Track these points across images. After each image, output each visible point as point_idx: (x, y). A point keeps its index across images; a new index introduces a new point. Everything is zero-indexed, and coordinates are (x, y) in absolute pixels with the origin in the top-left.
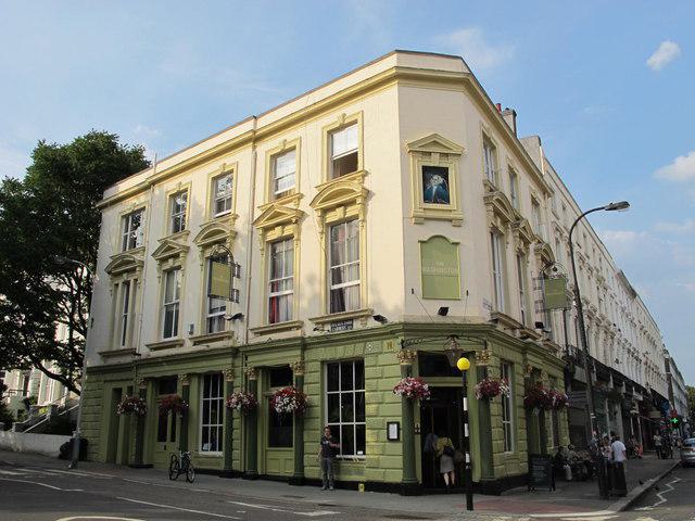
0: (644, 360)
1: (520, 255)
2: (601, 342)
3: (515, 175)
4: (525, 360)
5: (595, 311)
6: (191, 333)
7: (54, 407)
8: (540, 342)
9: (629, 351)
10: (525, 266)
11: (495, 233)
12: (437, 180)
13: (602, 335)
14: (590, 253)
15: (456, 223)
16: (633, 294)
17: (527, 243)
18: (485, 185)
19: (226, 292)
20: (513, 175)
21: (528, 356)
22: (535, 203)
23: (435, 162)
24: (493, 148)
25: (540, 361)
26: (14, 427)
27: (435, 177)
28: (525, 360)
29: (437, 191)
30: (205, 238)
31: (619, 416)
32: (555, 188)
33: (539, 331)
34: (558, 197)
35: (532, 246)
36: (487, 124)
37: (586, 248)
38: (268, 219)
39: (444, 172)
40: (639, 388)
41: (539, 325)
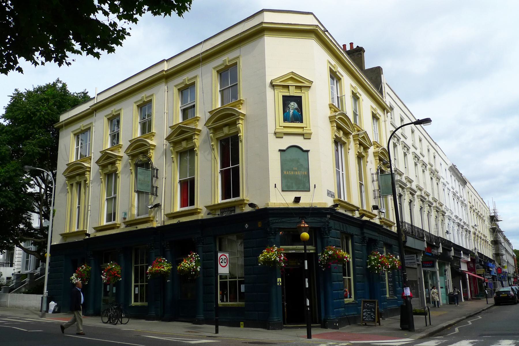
0: (472, 230)
1: (360, 157)
2: (433, 218)
3: (358, 98)
4: (363, 233)
5: (428, 196)
6: (125, 218)
7: (31, 274)
8: (376, 221)
9: (459, 225)
10: (365, 166)
11: (337, 142)
12: (293, 105)
13: (433, 213)
14: (425, 152)
15: (306, 136)
16: (464, 182)
17: (366, 148)
18: (330, 108)
19: (149, 190)
20: (355, 97)
21: (365, 231)
22: (375, 117)
23: (293, 92)
24: (339, 79)
25: (376, 234)
26: (2, 289)
27: (292, 103)
28: (363, 233)
29: (294, 114)
30: (215, 121)
31: (449, 273)
32: (394, 104)
33: (375, 212)
34: (397, 113)
35: (372, 150)
36: (334, 62)
37: (421, 149)
38: (104, 160)
39: (298, 100)
40: (467, 252)
41: (375, 208)
